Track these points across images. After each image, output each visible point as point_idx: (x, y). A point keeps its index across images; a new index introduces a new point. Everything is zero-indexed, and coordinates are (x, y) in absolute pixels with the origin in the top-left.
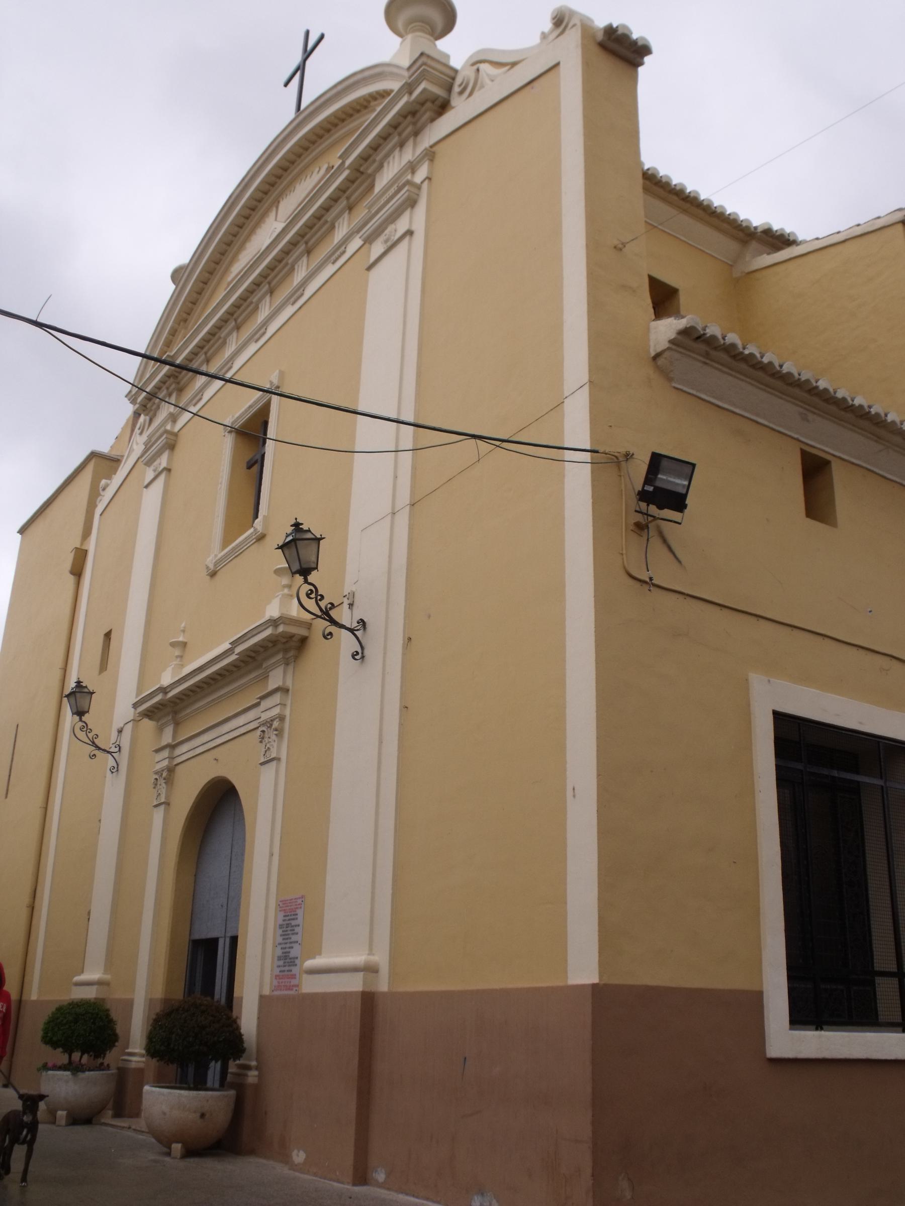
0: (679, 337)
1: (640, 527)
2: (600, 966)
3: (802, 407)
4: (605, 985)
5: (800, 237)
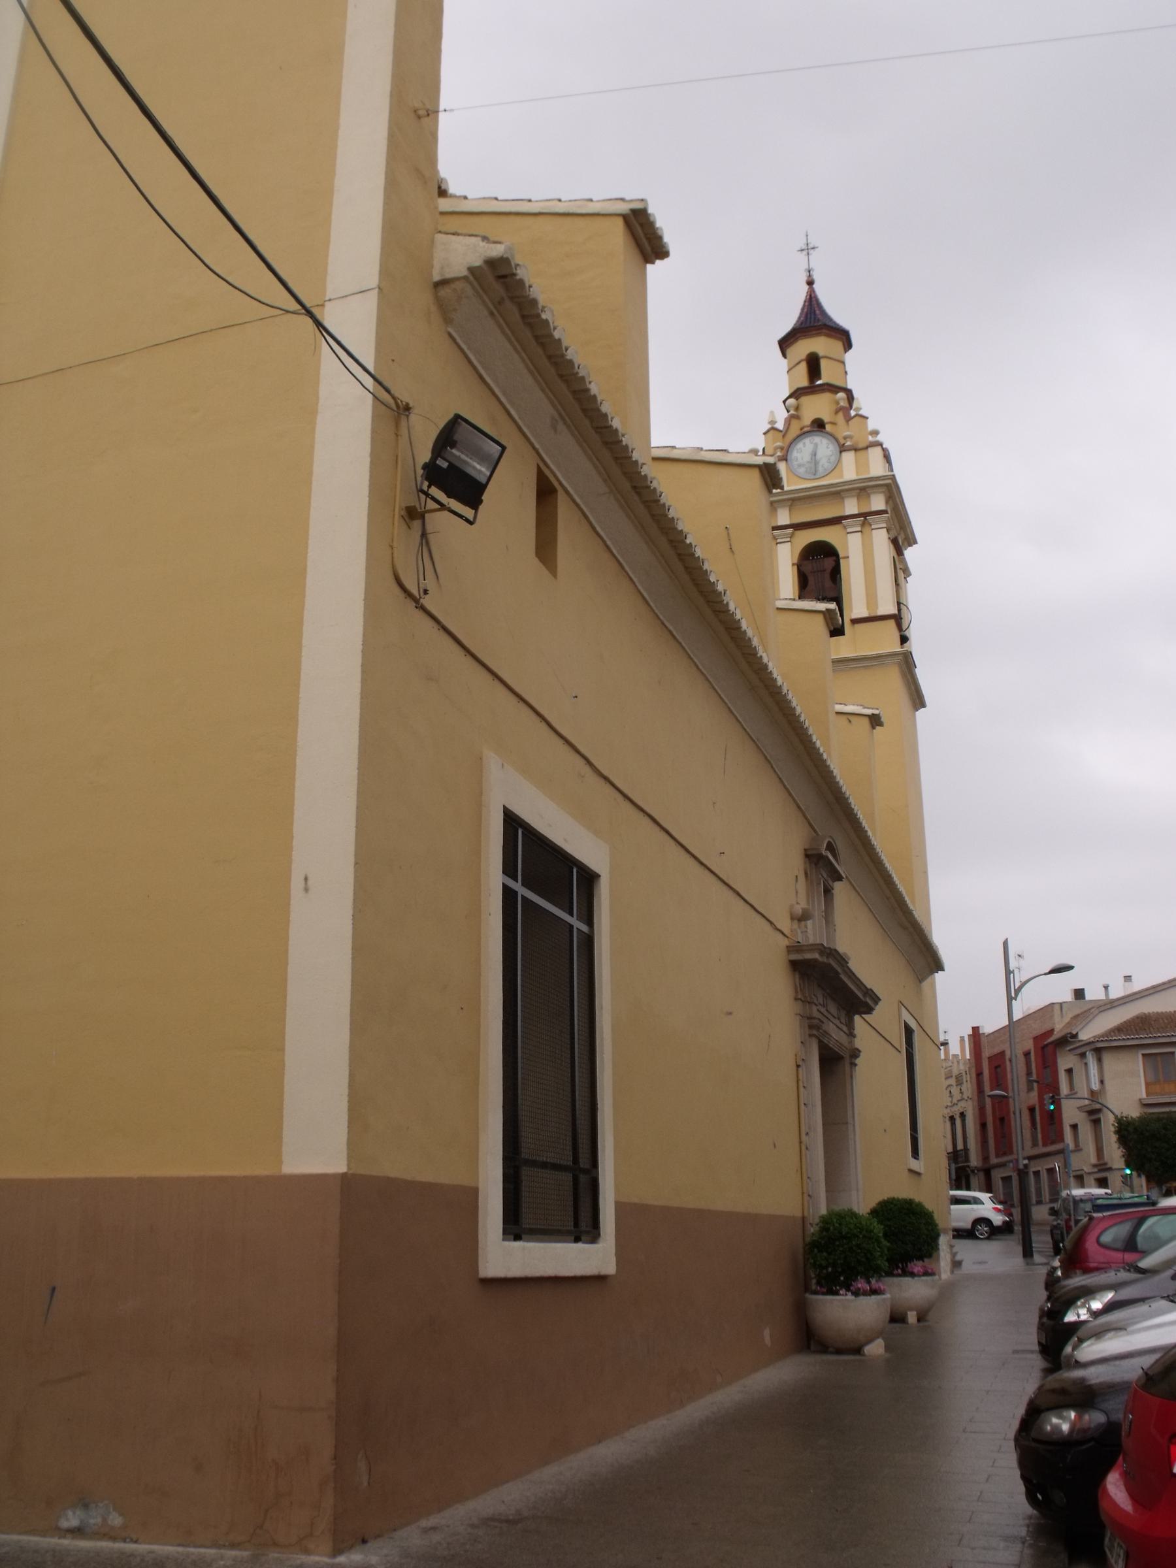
0: (485, 268)
1: (413, 514)
2: (348, 1149)
3: (557, 411)
4: (354, 1175)
5: (453, 189)
